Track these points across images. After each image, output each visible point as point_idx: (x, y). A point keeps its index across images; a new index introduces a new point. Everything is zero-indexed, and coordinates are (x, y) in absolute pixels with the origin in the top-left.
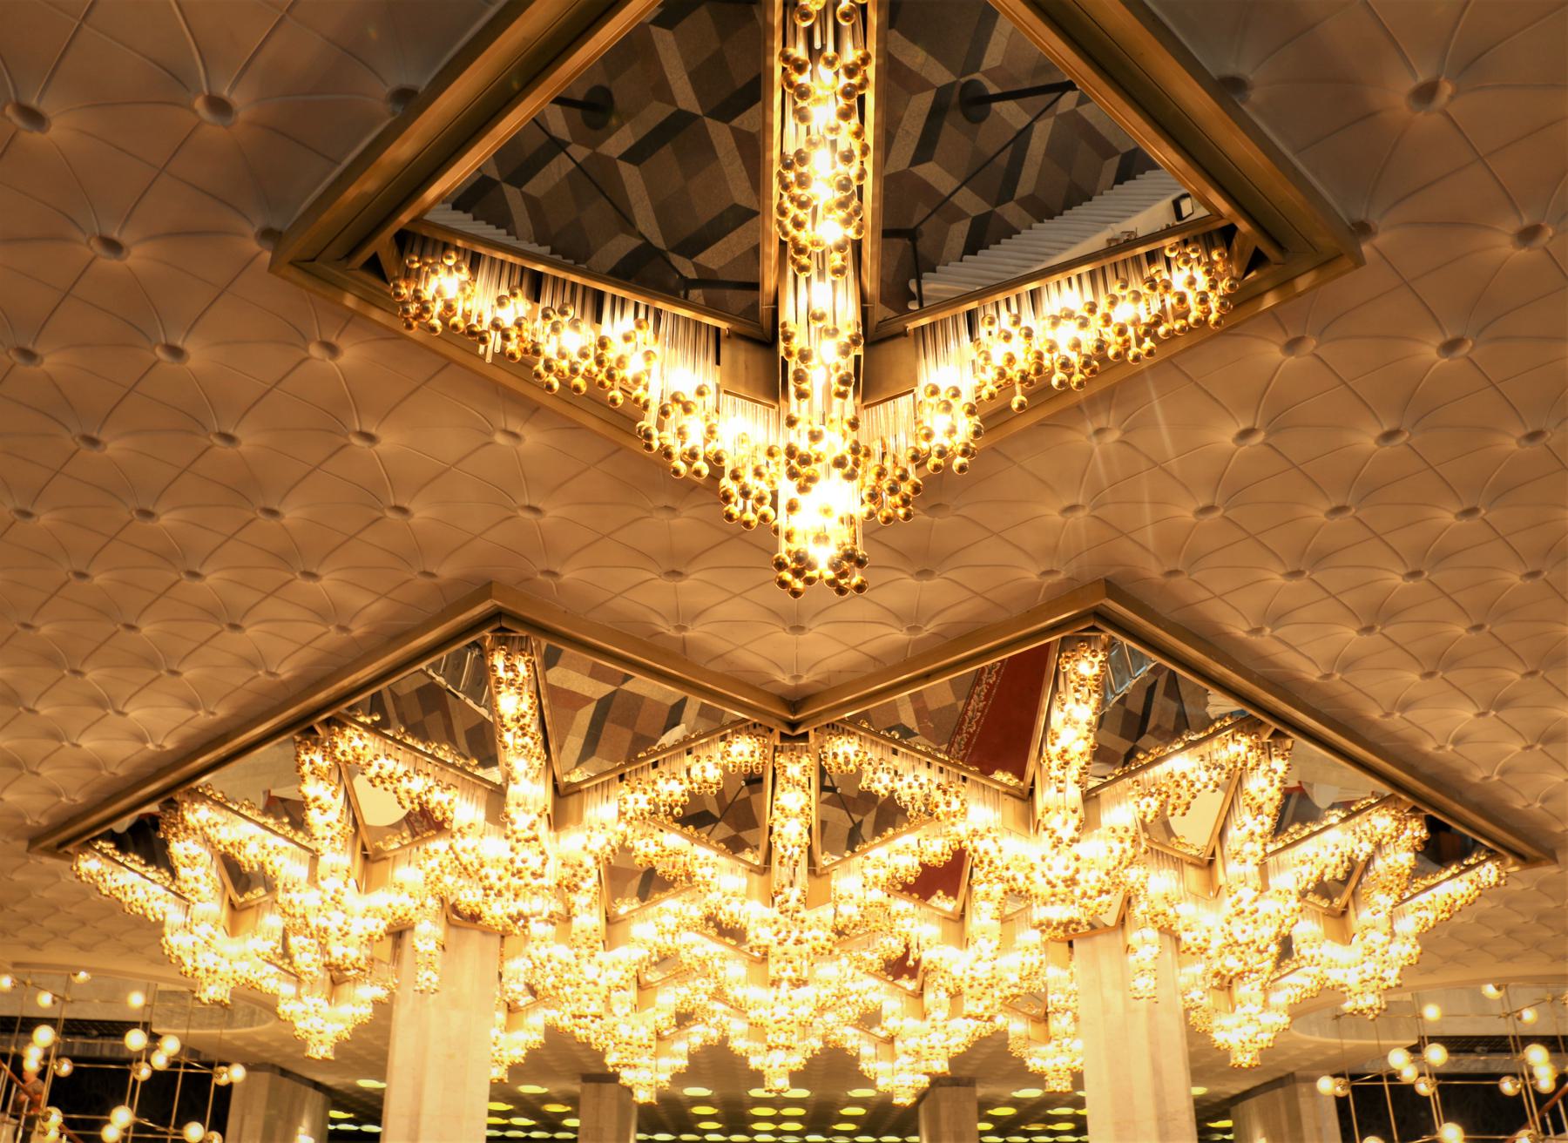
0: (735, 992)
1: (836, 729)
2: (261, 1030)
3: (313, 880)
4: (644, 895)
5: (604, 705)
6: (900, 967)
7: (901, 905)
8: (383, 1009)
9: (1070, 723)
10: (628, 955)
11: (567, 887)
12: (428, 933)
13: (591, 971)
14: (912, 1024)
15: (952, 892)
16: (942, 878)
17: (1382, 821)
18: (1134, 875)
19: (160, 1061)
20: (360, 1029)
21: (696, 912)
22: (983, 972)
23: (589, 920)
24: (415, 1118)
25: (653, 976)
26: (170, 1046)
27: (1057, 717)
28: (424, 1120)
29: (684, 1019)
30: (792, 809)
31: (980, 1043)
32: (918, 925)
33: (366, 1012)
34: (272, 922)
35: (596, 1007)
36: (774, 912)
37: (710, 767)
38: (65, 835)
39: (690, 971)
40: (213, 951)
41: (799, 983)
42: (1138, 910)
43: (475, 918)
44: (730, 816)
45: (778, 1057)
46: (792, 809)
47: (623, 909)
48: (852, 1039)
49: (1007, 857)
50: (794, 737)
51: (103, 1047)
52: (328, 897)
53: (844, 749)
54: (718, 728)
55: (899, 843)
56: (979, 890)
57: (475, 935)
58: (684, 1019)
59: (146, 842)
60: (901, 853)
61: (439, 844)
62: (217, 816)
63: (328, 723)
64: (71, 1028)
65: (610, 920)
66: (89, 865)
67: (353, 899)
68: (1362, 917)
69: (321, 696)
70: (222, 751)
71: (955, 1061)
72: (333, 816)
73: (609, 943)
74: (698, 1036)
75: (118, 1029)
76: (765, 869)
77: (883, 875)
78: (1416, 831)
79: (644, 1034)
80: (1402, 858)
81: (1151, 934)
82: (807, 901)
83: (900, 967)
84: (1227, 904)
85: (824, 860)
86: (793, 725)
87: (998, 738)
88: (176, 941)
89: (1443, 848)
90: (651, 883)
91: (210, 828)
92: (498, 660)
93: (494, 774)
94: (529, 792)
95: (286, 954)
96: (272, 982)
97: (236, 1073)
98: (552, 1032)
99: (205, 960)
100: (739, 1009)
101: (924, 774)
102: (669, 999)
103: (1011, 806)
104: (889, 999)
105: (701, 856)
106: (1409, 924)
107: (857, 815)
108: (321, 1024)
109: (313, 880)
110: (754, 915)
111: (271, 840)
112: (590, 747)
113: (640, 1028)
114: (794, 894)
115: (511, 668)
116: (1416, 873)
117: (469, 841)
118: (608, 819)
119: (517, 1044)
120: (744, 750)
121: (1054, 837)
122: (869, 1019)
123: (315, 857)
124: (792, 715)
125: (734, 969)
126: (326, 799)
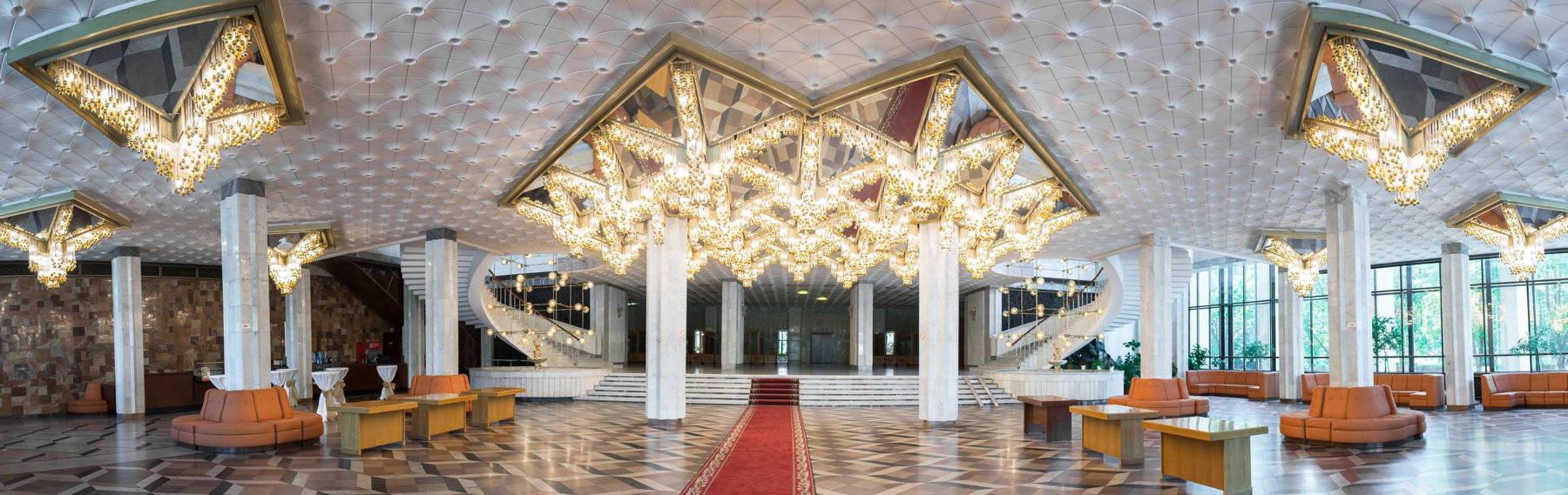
0: (784, 240)
1: (832, 115)
2: (599, 269)
3: (608, 199)
4: (747, 197)
5: (725, 115)
6: (851, 231)
7: (853, 203)
8: (643, 253)
9: (939, 114)
10: (739, 223)
11: (715, 189)
12: (658, 220)
13: (725, 230)
14: (854, 255)
15: (874, 199)
16: (870, 192)
17: (1048, 188)
18: (950, 195)
19: (563, 283)
20: (634, 261)
21: (768, 205)
22: (885, 232)
23: (723, 209)
24: (659, 292)
25: (750, 235)
26: (565, 277)
27: (932, 115)
28: (663, 289)
29: (762, 253)
30: (812, 152)
31: (878, 264)
32: (861, 213)
33: (636, 255)
34: (595, 221)
35: (728, 245)
36: (801, 202)
37: (771, 133)
38: (510, 197)
39: (765, 232)
40: (577, 235)
41: (812, 232)
42: (948, 212)
43: (676, 212)
44: (783, 159)
45: (800, 268)
46: (812, 152)
47: (737, 204)
48: (827, 261)
49: (903, 179)
50: (812, 117)
51: (543, 282)
52: (617, 203)
53: (835, 124)
54: (778, 112)
55: (855, 174)
56: (886, 198)
57: (677, 220)
58: (762, 253)
59: (542, 196)
60: (857, 177)
61: (659, 178)
62: (566, 177)
63: (604, 123)
64: (528, 276)
65: (732, 209)
66: (521, 207)
67: (625, 205)
68: (1031, 225)
69: (601, 108)
70: (562, 146)
71: (870, 270)
72: (612, 168)
73: (731, 218)
74: (768, 260)
75: (546, 274)
76: (798, 183)
77: (848, 187)
78: (1058, 193)
79: (747, 258)
80: (1051, 204)
81: (951, 223)
82: (816, 196)
83: (851, 231)
84: (985, 211)
85: (823, 180)
86: (813, 112)
87: (904, 119)
88: (560, 232)
89: (1065, 203)
90: (750, 191)
91: (565, 181)
92: (677, 77)
93: (680, 140)
94: (697, 146)
95: (602, 235)
96: (596, 244)
97: (590, 285)
98: (710, 259)
99: (571, 238)
100: (785, 247)
101: (870, 139)
102: (755, 245)
103: (907, 156)
104: (845, 245)
105: (772, 177)
106: (1046, 230)
107: (839, 157)
108: (620, 261)
109: (608, 199)
110: (794, 205)
111: (589, 184)
112: (721, 130)
113: (745, 256)
114: (809, 193)
115: (683, 80)
116: (1055, 211)
117: (671, 171)
118: (728, 158)
119: (696, 264)
120: (790, 124)
121: (920, 169)
122: (836, 253)
123: (607, 188)
124: (813, 107)
125: (783, 231)
126: (608, 160)
